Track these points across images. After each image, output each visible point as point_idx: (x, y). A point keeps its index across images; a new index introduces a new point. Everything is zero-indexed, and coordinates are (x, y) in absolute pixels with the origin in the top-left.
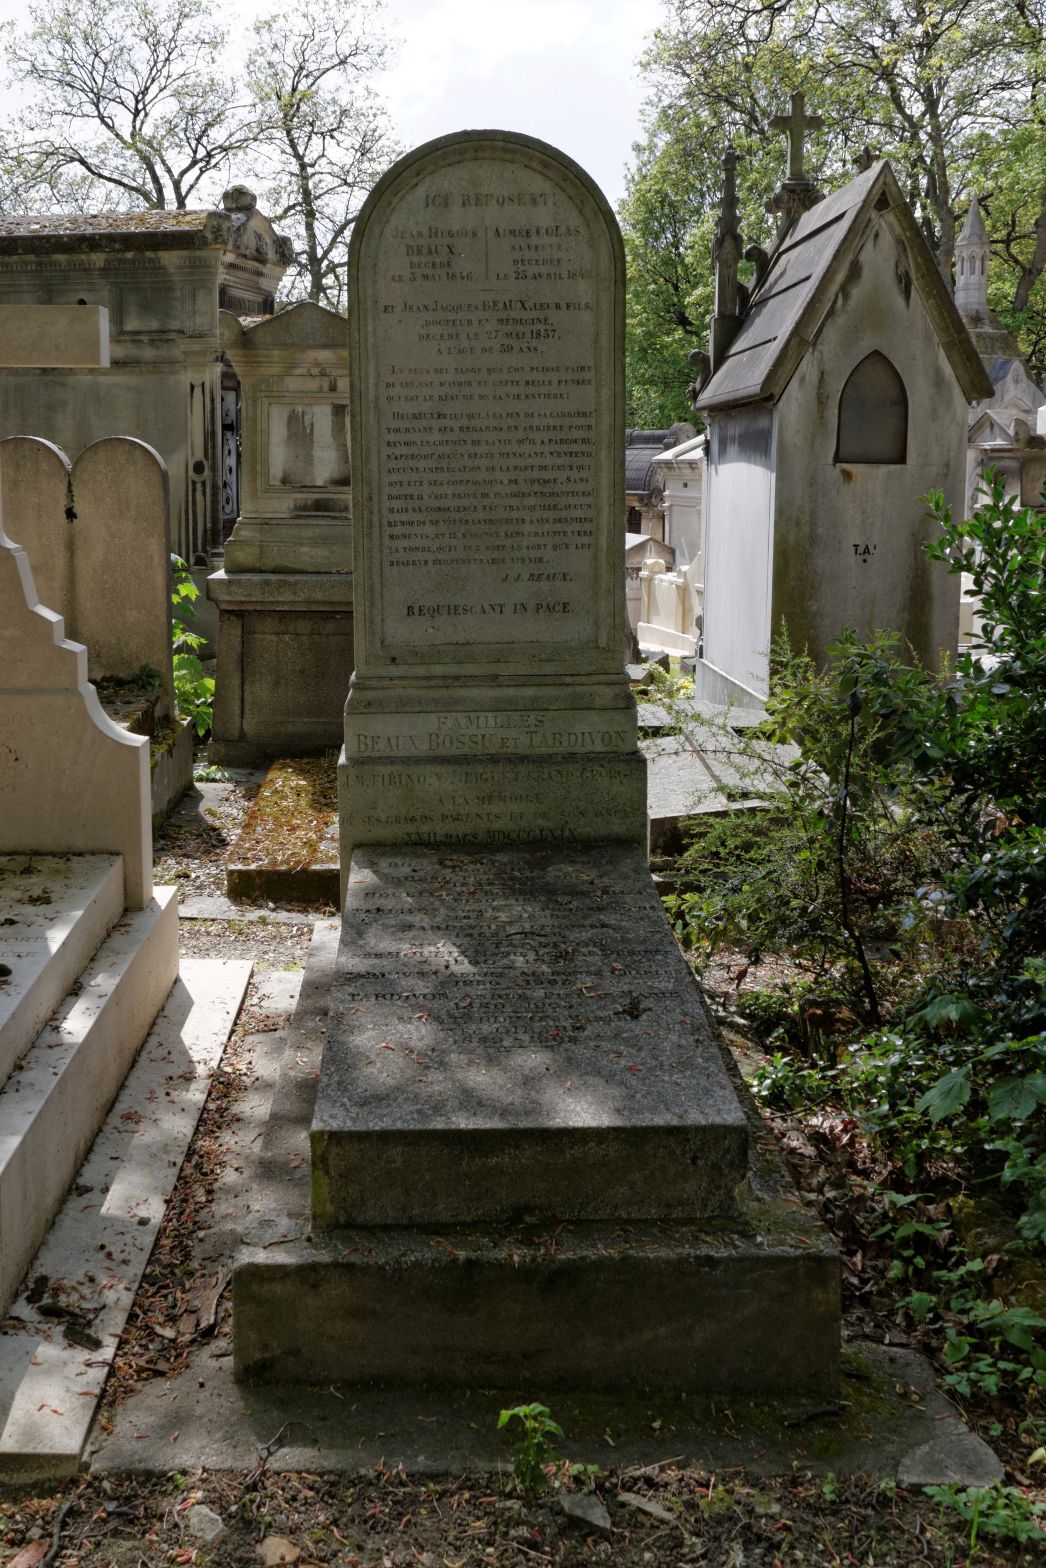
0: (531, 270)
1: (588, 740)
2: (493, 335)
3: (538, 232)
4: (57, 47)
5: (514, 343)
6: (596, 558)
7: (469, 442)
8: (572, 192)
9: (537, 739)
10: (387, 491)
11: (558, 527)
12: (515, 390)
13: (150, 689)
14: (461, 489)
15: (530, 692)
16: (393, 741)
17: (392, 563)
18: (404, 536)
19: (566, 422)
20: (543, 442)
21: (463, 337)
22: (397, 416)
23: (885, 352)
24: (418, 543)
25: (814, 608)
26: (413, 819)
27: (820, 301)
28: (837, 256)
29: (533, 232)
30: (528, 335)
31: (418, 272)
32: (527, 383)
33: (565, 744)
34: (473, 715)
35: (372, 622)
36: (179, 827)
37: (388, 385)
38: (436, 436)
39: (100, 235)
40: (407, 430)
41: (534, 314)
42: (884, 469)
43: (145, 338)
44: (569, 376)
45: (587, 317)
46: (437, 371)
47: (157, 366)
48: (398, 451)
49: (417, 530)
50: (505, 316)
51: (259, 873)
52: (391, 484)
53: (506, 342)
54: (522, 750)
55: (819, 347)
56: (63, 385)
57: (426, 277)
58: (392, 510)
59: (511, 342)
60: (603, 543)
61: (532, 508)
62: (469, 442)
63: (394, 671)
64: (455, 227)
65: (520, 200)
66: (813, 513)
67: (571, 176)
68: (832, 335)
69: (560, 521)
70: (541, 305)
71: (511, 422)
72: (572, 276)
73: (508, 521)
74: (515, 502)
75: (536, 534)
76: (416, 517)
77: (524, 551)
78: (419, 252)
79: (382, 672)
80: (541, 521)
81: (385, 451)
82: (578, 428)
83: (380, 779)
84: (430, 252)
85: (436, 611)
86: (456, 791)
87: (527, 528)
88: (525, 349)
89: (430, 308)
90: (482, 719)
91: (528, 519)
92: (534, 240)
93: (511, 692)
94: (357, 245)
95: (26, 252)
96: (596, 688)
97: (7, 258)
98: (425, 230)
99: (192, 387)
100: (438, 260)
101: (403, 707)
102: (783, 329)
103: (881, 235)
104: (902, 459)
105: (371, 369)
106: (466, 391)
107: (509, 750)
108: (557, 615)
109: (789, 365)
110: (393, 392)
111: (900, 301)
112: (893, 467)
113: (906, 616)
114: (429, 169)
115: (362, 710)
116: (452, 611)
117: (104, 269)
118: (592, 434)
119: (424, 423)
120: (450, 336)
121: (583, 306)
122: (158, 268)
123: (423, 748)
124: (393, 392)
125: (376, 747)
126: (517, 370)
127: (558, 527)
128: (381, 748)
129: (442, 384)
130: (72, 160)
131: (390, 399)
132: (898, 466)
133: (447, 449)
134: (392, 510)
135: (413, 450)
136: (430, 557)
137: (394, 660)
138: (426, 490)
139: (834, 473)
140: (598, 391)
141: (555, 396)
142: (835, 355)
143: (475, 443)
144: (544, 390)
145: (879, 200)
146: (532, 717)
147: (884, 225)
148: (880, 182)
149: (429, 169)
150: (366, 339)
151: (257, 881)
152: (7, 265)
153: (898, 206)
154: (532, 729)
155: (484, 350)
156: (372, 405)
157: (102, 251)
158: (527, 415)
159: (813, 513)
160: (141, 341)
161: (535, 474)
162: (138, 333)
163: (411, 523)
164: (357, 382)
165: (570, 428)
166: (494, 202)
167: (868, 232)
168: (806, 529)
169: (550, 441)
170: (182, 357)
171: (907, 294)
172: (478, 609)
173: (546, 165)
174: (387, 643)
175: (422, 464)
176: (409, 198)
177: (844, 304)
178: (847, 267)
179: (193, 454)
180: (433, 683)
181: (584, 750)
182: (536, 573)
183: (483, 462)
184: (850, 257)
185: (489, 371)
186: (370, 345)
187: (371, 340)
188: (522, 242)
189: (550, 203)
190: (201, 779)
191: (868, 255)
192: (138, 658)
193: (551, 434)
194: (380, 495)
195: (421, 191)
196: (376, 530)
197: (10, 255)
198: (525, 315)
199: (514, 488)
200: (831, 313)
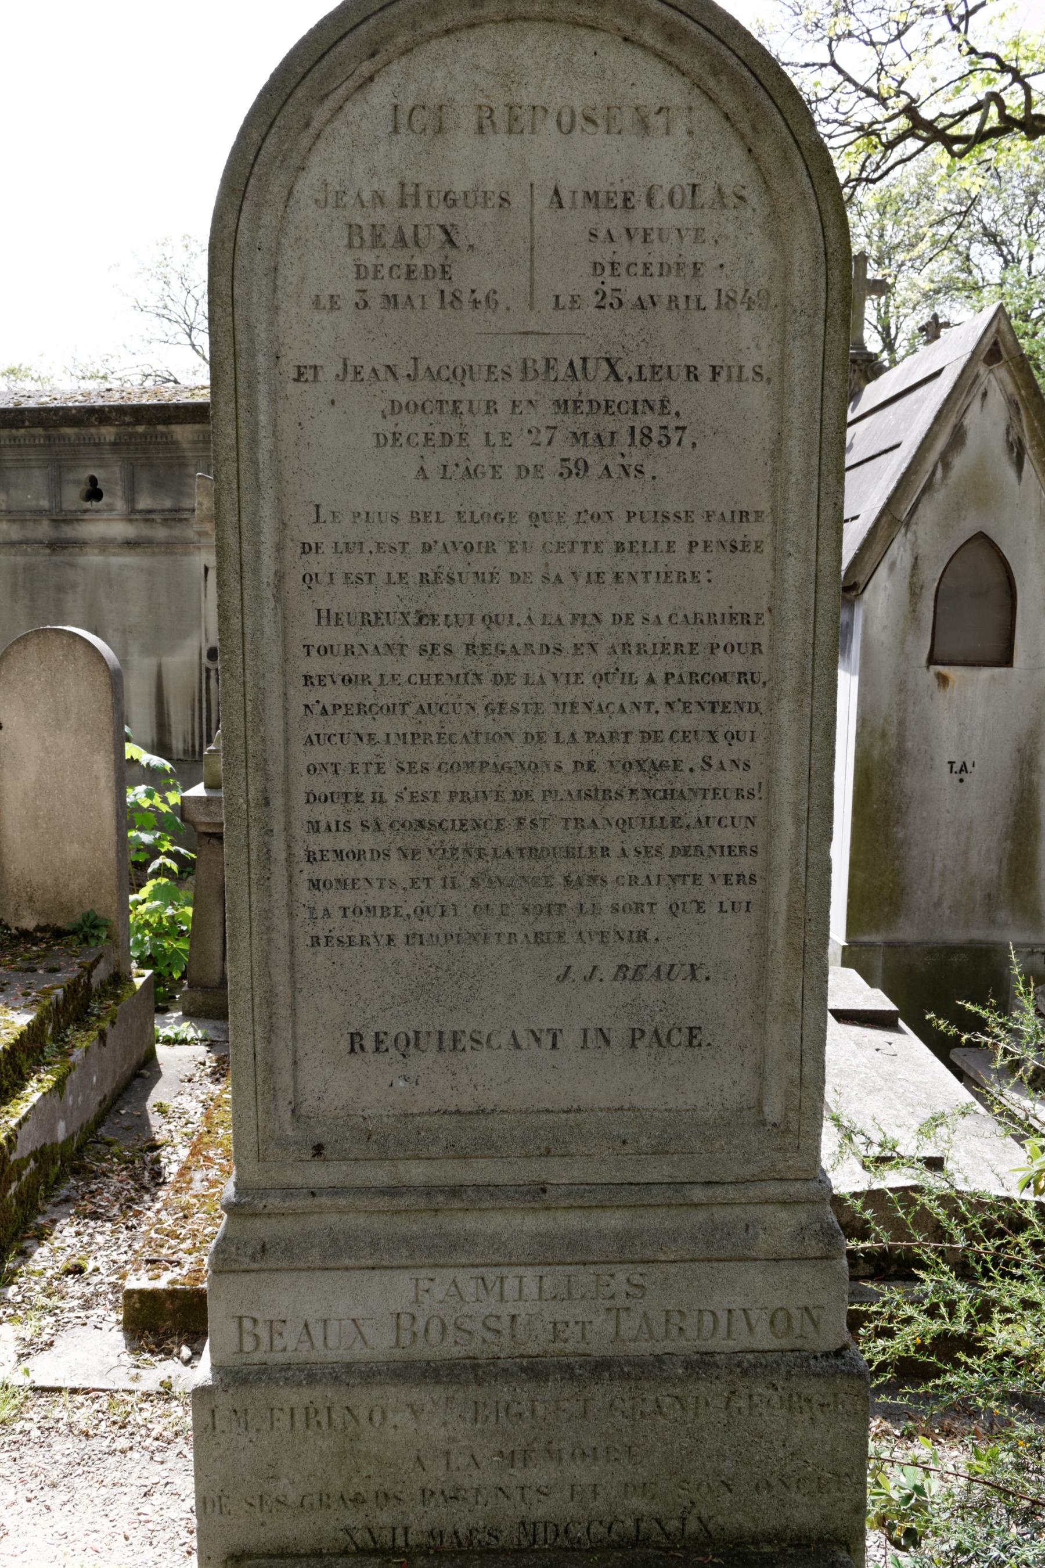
0: (633, 287)
1: (740, 1325)
2: (544, 438)
3: (650, 200)
4: (157, 286)
5: (593, 457)
6: (762, 933)
7: (487, 677)
8: (732, 103)
9: (630, 1325)
10: (303, 783)
11: (681, 865)
12: (591, 563)
13: (93, 943)
14: (468, 782)
15: (614, 1220)
16: (317, 1331)
17: (315, 941)
18: (342, 883)
19: (704, 635)
20: (651, 680)
21: (476, 440)
22: (326, 617)
23: (991, 534)
24: (374, 897)
25: (901, 835)
26: (358, 1500)
27: (916, 472)
28: (939, 417)
29: (639, 199)
30: (624, 438)
31: (375, 287)
32: (619, 547)
33: (691, 1333)
34: (491, 1274)
35: (271, 1069)
36: (109, 1144)
37: (306, 548)
38: (413, 664)
39: (110, 407)
40: (349, 650)
41: (639, 390)
42: (986, 673)
43: (157, 517)
44: (714, 532)
45: (756, 397)
46: (415, 517)
47: (169, 547)
48: (328, 695)
49: (370, 869)
50: (572, 394)
51: (172, 1294)
52: (312, 769)
53: (573, 453)
54: (599, 1347)
55: (913, 527)
56: (72, 565)
57: (391, 301)
58: (314, 826)
59: (584, 453)
60: (780, 902)
61: (625, 824)
62: (487, 677)
63: (319, 1174)
64: (461, 183)
65: (609, 122)
66: (901, 723)
67: (733, 61)
68: (928, 514)
69: (686, 852)
70: (655, 369)
71: (581, 634)
72: (726, 301)
73: (570, 852)
74: (587, 810)
75: (633, 880)
76: (369, 841)
77: (607, 916)
78: (377, 240)
79: (294, 1177)
80: (646, 852)
81: (300, 696)
82: (730, 648)
83: (285, 1418)
84: (402, 241)
85: (414, 1041)
86: (452, 1440)
87: (614, 867)
88: (616, 471)
89: (401, 372)
90: (511, 1283)
91: (615, 850)
92: (641, 217)
93: (573, 1221)
94: (230, 219)
95: (34, 425)
96: (757, 1212)
97: (14, 431)
98: (391, 192)
99: (206, 570)
100: (419, 262)
101: (337, 1253)
102: (868, 506)
103: (990, 394)
104: (1006, 660)
105: (267, 510)
106: (482, 563)
107: (569, 1347)
108: (676, 1054)
109: (877, 548)
110: (316, 564)
111: (1011, 473)
112: (997, 671)
113: (1008, 845)
114: (401, 40)
115: (246, 1263)
116: (448, 1043)
117: (114, 444)
118: (761, 663)
119: (386, 634)
120: (447, 438)
121: (748, 373)
122: (171, 444)
123: (380, 1344)
124: (316, 564)
125: (278, 1343)
126: (596, 517)
127: (681, 865)
128: (291, 1346)
129: (427, 548)
130: (169, 381)
131: (310, 579)
132: (1003, 670)
133: (439, 693)
134: (314, 826)
135: (364, 694)
136: (400, 929)
137: (318, 1150)
138: (391, 783)
139: (929, 676)
140: (776, 566)
141: (681, 576)
142: (931, 539)
143: (500, 679)
144: (656, 562)
145: (990, 350)
146: (621, 1277)
147: (994, 382)
148: (993, 329)
149: (401, 40)
150: (254, 442)
151: (168, 1305)
152: (15, 438)
153: (1012, 359)
154: (621, 1301)
155: (523, 471)
156: (268, 593)
157: (110, 425)
158: (617, 618)
159: (901, 723)
160: (153, 520)
161: (634, 750)
162: (150, 511)
163: (358, 855)
164: (232, 539)
165: (713, 648)
166: (551, 123)
167: (974, 390)
168: (893, 742)
169: (668, 676)
170: (196, 538)
171: (1019, 465)
172: (505, 1039)
173: (673, 35)
174: (304, 1110)
175: (381, 726)
176: (353, 110)
177: (945, 476)
178: (948, 431)
179: (207, 640)
180: (404, 1202)
181: (732, 1345)
182: (631, 963)
183: (518, 723)
184: (953, 420)
185: (535, 518)
186: (263, 456)
187: (266, 444)
188: (613, 221)
189: (679, 130)
190: (169, 1041)
191: (973, 419)
192: (80, 903)
193: (670, 663)
194: (287, 793)
195: (380, 95)
196: (279, 872)
197: (17, 428)
198: (617, 392)
199: (588, 780)
200: (928, 487)
